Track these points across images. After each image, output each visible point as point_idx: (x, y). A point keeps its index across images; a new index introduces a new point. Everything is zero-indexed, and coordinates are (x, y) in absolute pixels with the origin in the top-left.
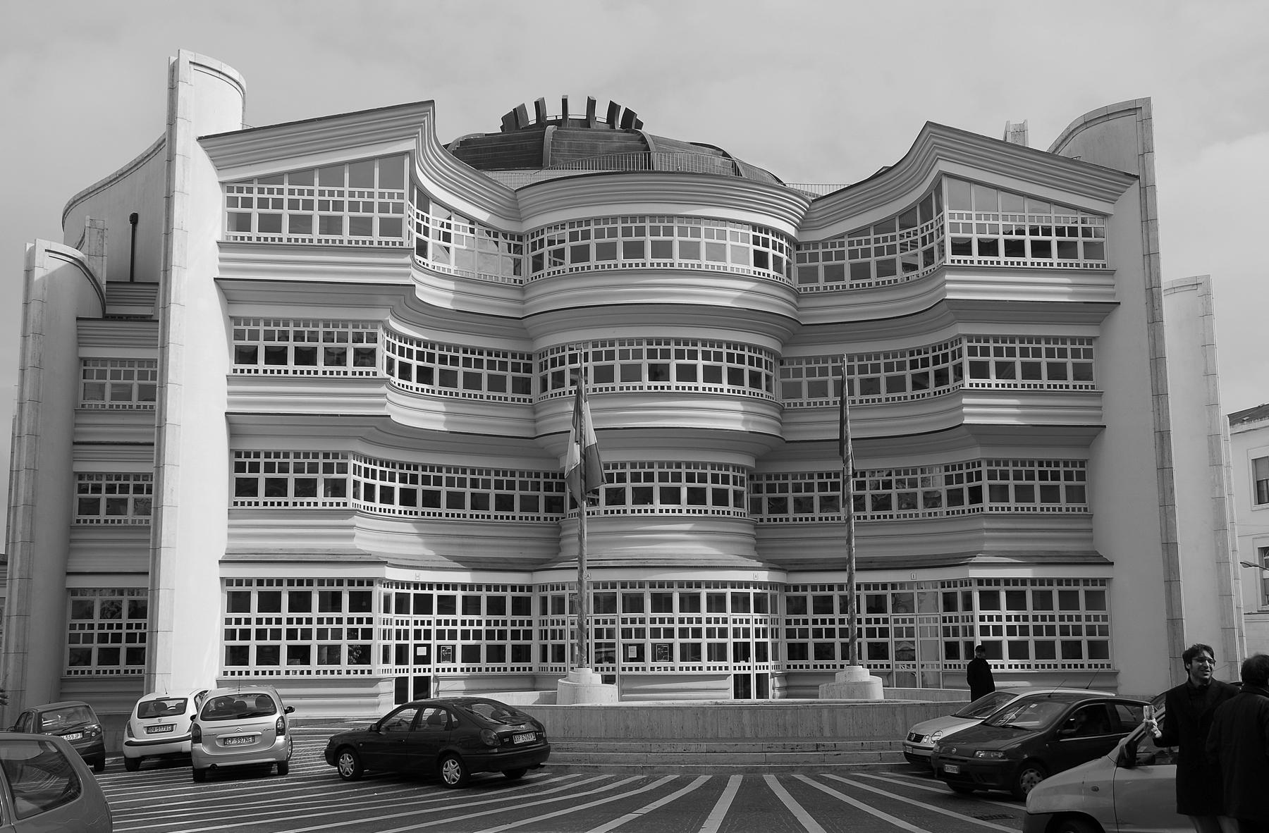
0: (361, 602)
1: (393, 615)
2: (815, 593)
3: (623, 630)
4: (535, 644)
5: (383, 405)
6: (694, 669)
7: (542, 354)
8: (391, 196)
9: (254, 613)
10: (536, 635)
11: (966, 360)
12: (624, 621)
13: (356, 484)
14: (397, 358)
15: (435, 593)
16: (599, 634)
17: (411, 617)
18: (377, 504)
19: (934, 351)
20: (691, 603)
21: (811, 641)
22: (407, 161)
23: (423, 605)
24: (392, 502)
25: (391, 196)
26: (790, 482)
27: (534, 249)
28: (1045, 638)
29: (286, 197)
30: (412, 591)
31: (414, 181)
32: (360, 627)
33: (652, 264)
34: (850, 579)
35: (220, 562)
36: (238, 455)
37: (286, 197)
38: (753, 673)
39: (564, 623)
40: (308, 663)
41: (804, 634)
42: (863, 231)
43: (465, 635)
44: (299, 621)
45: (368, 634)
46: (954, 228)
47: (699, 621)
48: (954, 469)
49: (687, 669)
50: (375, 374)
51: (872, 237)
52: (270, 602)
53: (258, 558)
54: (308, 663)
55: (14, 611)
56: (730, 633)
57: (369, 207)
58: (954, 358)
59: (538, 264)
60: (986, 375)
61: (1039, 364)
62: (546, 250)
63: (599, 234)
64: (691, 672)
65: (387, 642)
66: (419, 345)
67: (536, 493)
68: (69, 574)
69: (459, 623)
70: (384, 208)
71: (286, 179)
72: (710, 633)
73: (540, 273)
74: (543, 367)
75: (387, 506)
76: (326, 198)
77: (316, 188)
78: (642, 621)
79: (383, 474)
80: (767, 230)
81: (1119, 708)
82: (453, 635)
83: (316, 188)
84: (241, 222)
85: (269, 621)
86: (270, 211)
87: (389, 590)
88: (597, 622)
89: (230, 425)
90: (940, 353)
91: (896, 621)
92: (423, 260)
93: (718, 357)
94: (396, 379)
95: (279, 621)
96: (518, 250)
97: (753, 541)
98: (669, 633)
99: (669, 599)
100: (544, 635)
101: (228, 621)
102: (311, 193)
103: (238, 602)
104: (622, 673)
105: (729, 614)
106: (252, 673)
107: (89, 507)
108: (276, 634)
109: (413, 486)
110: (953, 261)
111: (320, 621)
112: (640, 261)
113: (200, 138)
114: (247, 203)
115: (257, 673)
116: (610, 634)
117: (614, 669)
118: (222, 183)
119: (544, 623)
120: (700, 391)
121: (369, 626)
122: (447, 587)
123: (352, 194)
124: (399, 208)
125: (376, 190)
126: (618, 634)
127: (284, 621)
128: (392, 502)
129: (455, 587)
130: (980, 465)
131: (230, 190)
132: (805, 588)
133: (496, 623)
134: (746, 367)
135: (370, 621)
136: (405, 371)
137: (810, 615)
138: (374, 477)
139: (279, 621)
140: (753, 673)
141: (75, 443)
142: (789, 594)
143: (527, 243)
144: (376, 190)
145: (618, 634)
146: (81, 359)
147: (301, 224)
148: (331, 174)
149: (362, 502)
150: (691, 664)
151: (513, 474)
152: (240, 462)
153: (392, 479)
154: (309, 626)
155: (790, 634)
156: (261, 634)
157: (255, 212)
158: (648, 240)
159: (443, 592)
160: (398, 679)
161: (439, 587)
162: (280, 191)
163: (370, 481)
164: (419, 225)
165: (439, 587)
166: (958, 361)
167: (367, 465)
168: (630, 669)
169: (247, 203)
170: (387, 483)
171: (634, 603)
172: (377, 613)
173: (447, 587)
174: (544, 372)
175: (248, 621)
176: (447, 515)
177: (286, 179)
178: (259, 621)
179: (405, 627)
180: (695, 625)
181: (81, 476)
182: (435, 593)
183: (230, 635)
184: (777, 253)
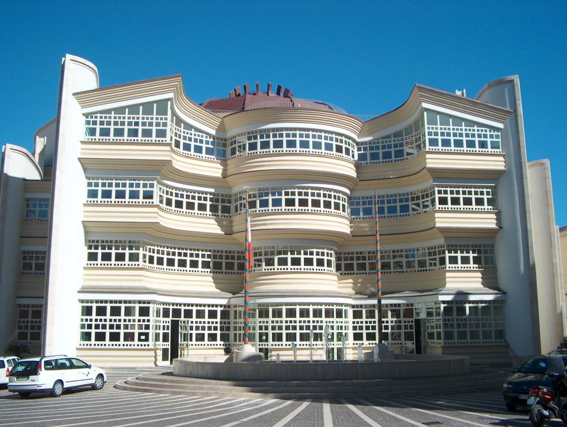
0: (144, 312)
1: (161, 319)
2: (33, 309)
3: (272, 326)
4: (151, 332)
5: (156, 217)
6: (116, 345)
7: (236, 195)
8: (161, 119)
9: (94, 316)
10: (232, 329)
11: (437, 196)
12: (273, 322)
13: (144, 256)
14: (165, 196)
15: (183, 308)
16: (261, 328)
17: (335, 319)
18: (155, 265)
19: (422, 192)
20: (291, 313)
21: (364, 332)
22: (169, 102)
23: (329, 314)
24: (162, 265)
25: (162, 119)
26: (404, 253)
27: (232, 145)
28: (371, 331)
29: (112, 120)
30: (171, 307)
31: (174, 114)
32: (115, 323)
33: (286, 151)
34: (379, 301)
35: (78, 292)
36: (90, 241)
37: (112, 120)
38: (335, 347)
39: (342, 322)
40: (90, 340)
41: (361, 328)
42: (389, 137)
43: (210, 328)
44: (277, 322)
45: (147, 327)
46: (430, 134)
47: (27, 322)
48: (432, 249)
49: (275, 345)
50: (153, 203)
51: (392, 139)
52: (101, 311)
53: (109, 290)
54: (90, 340)
55: (566, 317)
56: (403, 327)
57: (151, 124)
58: (431, 196)
59: (233, 152)
60: (483, 204)
61: (447, 198)
62: (236, 145)
63: (288, 135)
64: (277, 347)
65: (158, 331)
66: (176, 190)
67: (221, 260)
68: (17, 297)
69: (206, 323)
70: (158, 124)
71: (113, 112)
72: (197, 328)
73: (234, 156)
74: (236, 201)
75: (160, 267)
76: (159, 121)
77: (127, 116)
78: (281, 322)
79: (158, 251)
80: (342, 135)
81: (72, 360)
82: (203, 328)
83: (127, 116)
84: (92, 132)
85: (213, 323)
86: (147, 127)
87: (159, 306)
88: (326, 322)
89: (85, 227)
90: (425, 193)
91: (326, 322)
92: (178, 149)
93: (319, 195)
94: (164, 206)
95: (120, 320)
96: (225, 145)
97: (352, 285)
98: (203, 328)
99: (267, 312)
100: (235, 329)
101: (82, 320)
102: (138, 118)
103: (87, 311)
104: (271, 347)
105: (324, 319)
106: (93, 345)
107: (27, 266)
108: (104, 327)
109: (173, 257)
110: (429, 149)
111: (366, 322)
112: (280, 149)
113: (74, 94)
114: (95, 123)
115: (138, 345)
116: (267, 328)
117: (268, 345)
118: (84, 115)
119: (235, 323)
120: (310, 211)
121: (148, 323)
122: (188, 305)
123: (129, 118)
124: (165, 125)
125: (141, 116)
126: (270, 328)
127: (122, 321)
128: (162, 265)
129: (192, 305)
130: (33, 254)
131: (87, 117)
132: (28, 306)
133: (144, 321)
134: (333, 200)
135: (148, 321)
136: (169, 202)
137: (108, 317)
138: (154, 252)
139: (105, 320)
140: (335, 347)
141: (21, 237)
142: (21, 309)
143: (229, 142)
144: (141, 116)
145: (270, 328)
146: (26, 198)
147: (133, 133)
148: (134, 109)
149: (147, 264)
150: (277, 343)
151: (480, 246)
152: (91, 244)
153: (163, 254)
154: (119, 323)
155: (355, 328)
156: (97, 327)
157: (98, 127)
158: (271, 140)
159: (199, 308)
160: (163, 349)
161: (185, 305)
162: (110, 118)
163: (151, 254)
164: (176, 133)
165: (185, 305)
166: (433, 197)
167: (159, 248)
168: (127, 345)
169: (95, 123)
170: (160, 256)
171: (278, 313)
172: (152, 317)
173: (188, 305)
174: (237, 203)
175: (295, 322)
176: (202, 272)
177: (113, 112)
178: (111, 320)
179: (341, 324)
180: (279, 324)
181: (24, 252)
182: (183, 308)
183: (83, 327)
184: (347, 146)
